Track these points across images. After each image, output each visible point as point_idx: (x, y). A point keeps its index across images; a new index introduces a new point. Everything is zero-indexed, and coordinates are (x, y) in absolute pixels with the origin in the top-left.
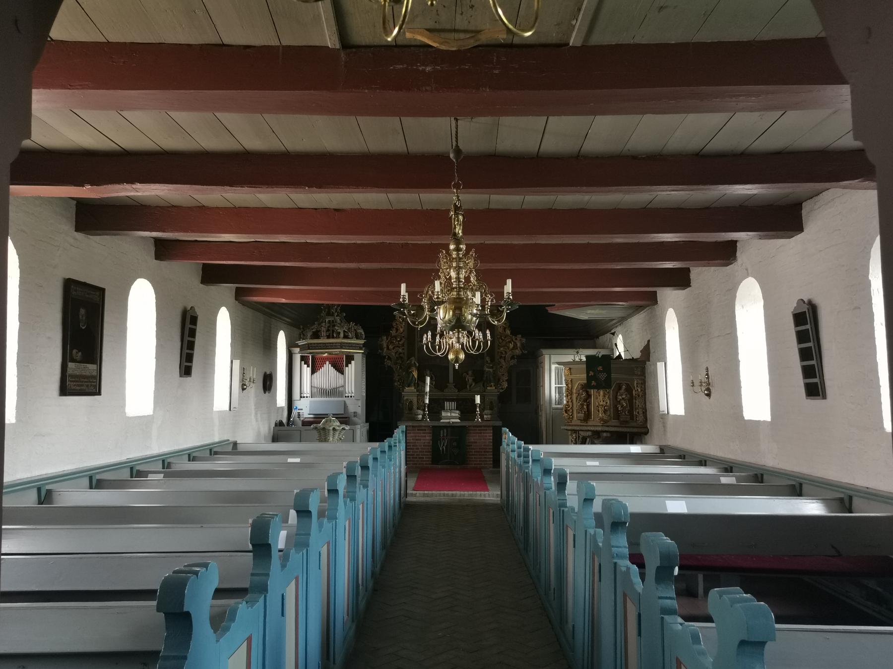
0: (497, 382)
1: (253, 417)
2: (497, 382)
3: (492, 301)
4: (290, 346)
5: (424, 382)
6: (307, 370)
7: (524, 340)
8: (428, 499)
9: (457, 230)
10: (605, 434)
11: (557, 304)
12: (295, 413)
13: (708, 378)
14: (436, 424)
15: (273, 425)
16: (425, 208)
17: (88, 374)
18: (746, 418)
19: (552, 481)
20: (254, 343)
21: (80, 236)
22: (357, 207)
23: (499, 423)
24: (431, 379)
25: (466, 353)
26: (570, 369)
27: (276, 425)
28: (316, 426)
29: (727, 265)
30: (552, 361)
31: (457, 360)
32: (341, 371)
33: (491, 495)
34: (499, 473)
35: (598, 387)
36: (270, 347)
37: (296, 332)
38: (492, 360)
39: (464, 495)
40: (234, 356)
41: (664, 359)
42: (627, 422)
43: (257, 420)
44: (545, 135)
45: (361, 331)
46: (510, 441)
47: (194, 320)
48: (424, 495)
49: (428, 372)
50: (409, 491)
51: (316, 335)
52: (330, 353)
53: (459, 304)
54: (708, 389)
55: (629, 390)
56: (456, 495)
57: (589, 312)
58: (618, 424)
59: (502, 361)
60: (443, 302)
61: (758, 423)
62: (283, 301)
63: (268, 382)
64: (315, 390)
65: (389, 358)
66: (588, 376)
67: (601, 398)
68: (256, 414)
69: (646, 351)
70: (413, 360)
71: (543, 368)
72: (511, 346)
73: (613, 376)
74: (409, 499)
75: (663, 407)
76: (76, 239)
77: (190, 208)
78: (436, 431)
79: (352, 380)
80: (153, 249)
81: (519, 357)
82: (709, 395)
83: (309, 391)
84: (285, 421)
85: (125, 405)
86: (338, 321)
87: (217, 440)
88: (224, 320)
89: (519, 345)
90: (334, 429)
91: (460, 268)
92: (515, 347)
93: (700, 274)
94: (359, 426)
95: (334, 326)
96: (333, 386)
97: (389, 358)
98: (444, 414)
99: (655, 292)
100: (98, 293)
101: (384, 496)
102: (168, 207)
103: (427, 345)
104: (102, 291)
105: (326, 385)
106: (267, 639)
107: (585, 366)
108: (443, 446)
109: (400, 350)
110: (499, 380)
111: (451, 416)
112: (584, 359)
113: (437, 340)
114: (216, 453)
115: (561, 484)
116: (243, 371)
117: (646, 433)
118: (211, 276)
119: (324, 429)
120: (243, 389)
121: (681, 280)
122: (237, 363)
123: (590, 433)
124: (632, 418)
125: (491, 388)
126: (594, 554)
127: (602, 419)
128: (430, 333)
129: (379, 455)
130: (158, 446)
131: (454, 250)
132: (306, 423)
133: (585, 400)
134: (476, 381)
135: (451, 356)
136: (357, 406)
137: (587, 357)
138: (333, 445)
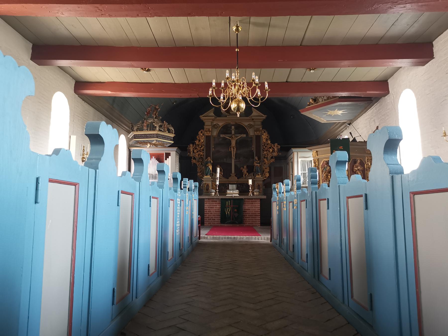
0: (263, 173)
2: (263, 173)
5: (216, 172)
24: (221, 170)
26: (317, 152)
30: (299, 156)
31: (238, 108)
38: (259, 159)
39: (243, 238)
45: (171, 128)
51: (142, 130)
59: (265, 160)
65: (194, 158)
70: (209, 159)
71: (292, 163)
72: (271, 150)
74: (202, 240)
78: (223, 202)
81: (277, 158)
89: (276, 149)
92: (273, 151)
97: (194, 158)
98: (228, 192)
108: (228, 211)
110: (263, 172)
111: (233, 192)
125: (259, 176)
135: (233, 106)
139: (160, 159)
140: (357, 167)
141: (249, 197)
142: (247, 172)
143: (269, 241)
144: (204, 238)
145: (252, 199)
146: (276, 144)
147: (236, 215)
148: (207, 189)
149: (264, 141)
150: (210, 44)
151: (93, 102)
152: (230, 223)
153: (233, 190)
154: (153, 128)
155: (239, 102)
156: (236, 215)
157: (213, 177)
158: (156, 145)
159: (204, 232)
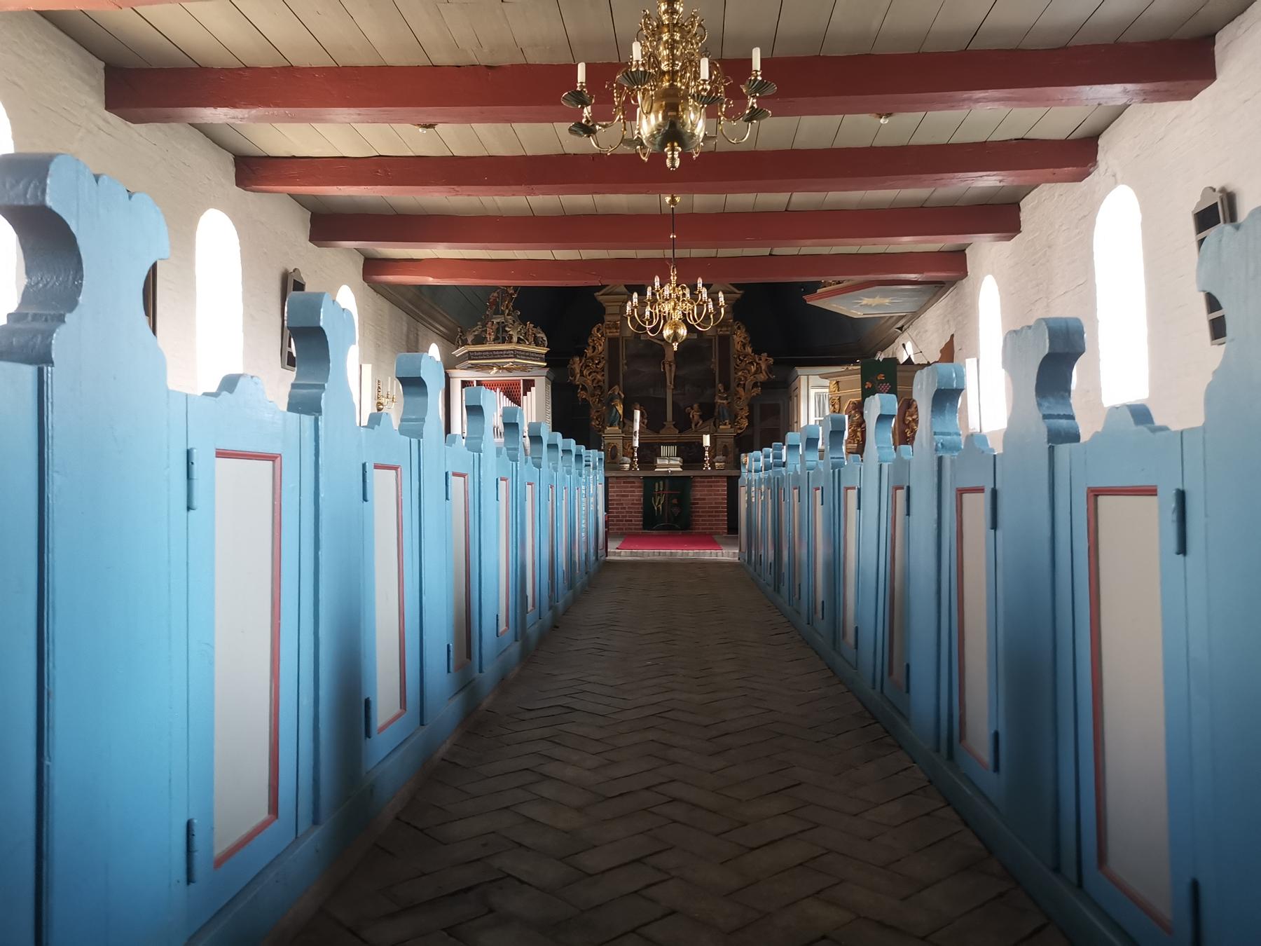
0: (734, 420)
2: (734, 420)
7: (771, 361)
25: (690, 328)
29: (1080, 178)
31: (675, 337)
38: (727, 388)
41: (975, 353)
51: (480, 340)
57: (865, 301)
59: (740, 390)
62: (431, 281)
65: (584, 388)
70: (617, 390)
71: (798, 396)
72: (753, 369)
76: (105, 120)
77: (272, 71)
78: (649, 483)
81: (764, 385)
92: (758, 371)
97: (584, 388)
98: (659, 461)
102: (240, 69)
103: (633, 318)
106: (322, 495)
108: (658, 504)
109: (599, 377)
110: (736, 416)
111: (669, 463)
118: (328, 225)
121: (1001, 217)
131: (666, 12)
134: (704, 418)
135: (667, 332)
139: (513, 393)
142: (701, 417)
145: (711, 477)
147: (676, 511)
149: (738, 347)
150: (626, 212)
151: (391, 294)
152: (664, 528)
153: (669, 457)
154: (507, 339)
155: (676, 326)
156: (676, 511)
158: (509, 370)
159: (613, 546)
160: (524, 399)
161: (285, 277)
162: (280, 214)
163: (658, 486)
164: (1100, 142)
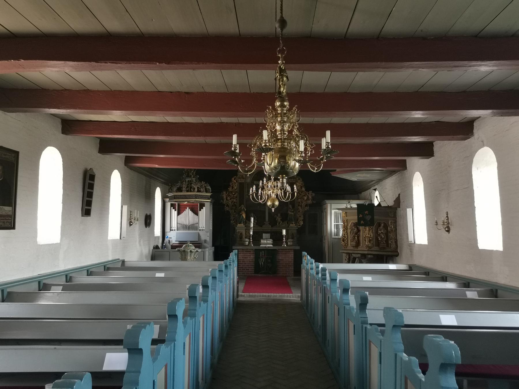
0: (297, 221)
1: (137, 243)
2: (297, 221)
3: (311, 151)
4: (164, 197)
5: (250, 220)
6: (175, 213)
7: (314, 194)
8: (253, 299)
9: (282, 89)
10: (369, 256)
11: (338, 170)
12: (166, 240)
13: (448, 219)
14: (257, 247)
15: (152, 248)
16: (252, 92)
17: (4, 213)
18: (480, 248)
19: (352, 301)
20: (138, 194)
21: (99, 154)
22: (201, 90)
23: (298, 248)
25: (280, 201)
26: (346, 213)
27: (154, 248)
28: (179, 250)
30: (332, 207)
31: (273, 205)
32: (196, 213)
33: (294, 296)
34: (300, 280)
35: (365, 225)
36: (150, 198)
37: (167, 187)
38: (293, 207)
39: (276, 296)
40: (123, 203)
41: (411, 206)
42: (384, 248)
43: (140, 245)
44: (356, 13)
45: (209, 187)
46: (308, 260)
47: (92, 177)
48: (250, 296)
49: (252, 215)
50: (240, 293)
51: (180, 190)
52: (188, 202)
53: (283, 154)
54: (448, 227)
55: (386, 227)
56: (271, 296)
57: (359, 175)
58: (378, 249)
59: (300, 207)
60: (271, 150)
61: (491, 252)
62: (157, 166)
63: (148, 221)
64: (179, 226)
65: (228, 206)
66: (358, 218)
67: (367, 232)
68: (140, 241)
69: (398, 201)
70: (243, 207)
72: (305, 198)
73: (375, 217)
74: (241, 299)
75: (411, 239)
77: (78, 91)
78: (257, 252)
79: (204, 219)
80: (60, 127)
81: (310, 206)
82: (448, 231)
83: (176, 226)
84: (160, 245)
85: (36, 237)
86: (194, 181)
87: (110, 259)
88: (116, 180)
89: (310, 197)
90: (191, 251)
91: (284, 122)
92: (308, 199)
93: (444, 147)
94: (207, 249)
95: (191, 184)
96: (192, 223)
97: (228, 206)
98: (262, 241)
99: (405, 161)
100: (13, 155)
101: (221, 297)
102: (62, 90)
103: (253, 195)
104: (16, 154)
105: (186, 223)
107: (356, 211)
108: (262, 262)
109: (235, 200)
110: (297, 220)
111: (267, 243)
112: (355, 206)
113: (260, 192)
114: (109, 269)
115: (363, 304)
116: (130, 214)
117: (397, 256)
118: (106, 147)
119: (184, 251)
120: (130, 225)
121: (425, 151)
122: (125, 208)
123: (359, 255)
124: (388, 246)
125: (293, 225)
126: (406, 379)
127: (367, 246)
128: (254, 187)
129: (217, 274)
130: (63, 265)
132: (173, 247)
133: (356, 233)
134: (283, 220)
135: (269, 203)
136: (207, 236)
137: (358, 205)
138: (190, 263)
140: (381, 230)
141: (283, 248)
143: (300, 299)
144: (242, 296)
145: (286, 250)
146: (310, 192)
148: (241, 238)
157: (247, 225)
160: (200, 213)
161: (85, 172)
162: (85, 145)
163: (262, 254)
164: (475, 124)
